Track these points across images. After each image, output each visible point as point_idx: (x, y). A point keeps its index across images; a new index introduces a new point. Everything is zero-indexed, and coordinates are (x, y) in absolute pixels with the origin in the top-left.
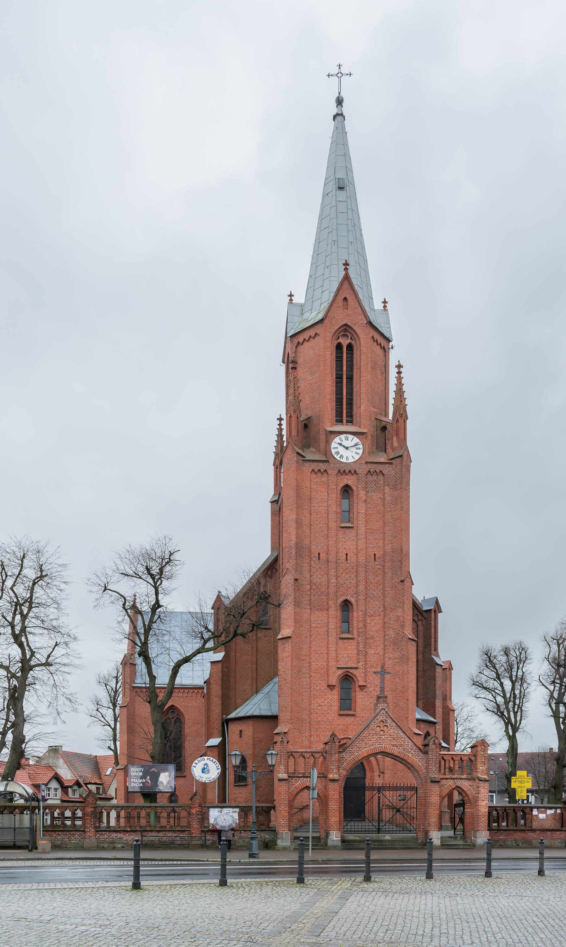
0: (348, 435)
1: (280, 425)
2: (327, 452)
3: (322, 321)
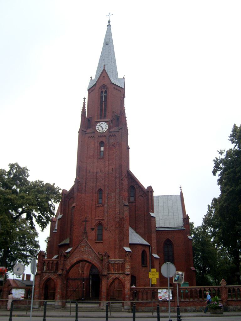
1: (84, 101)
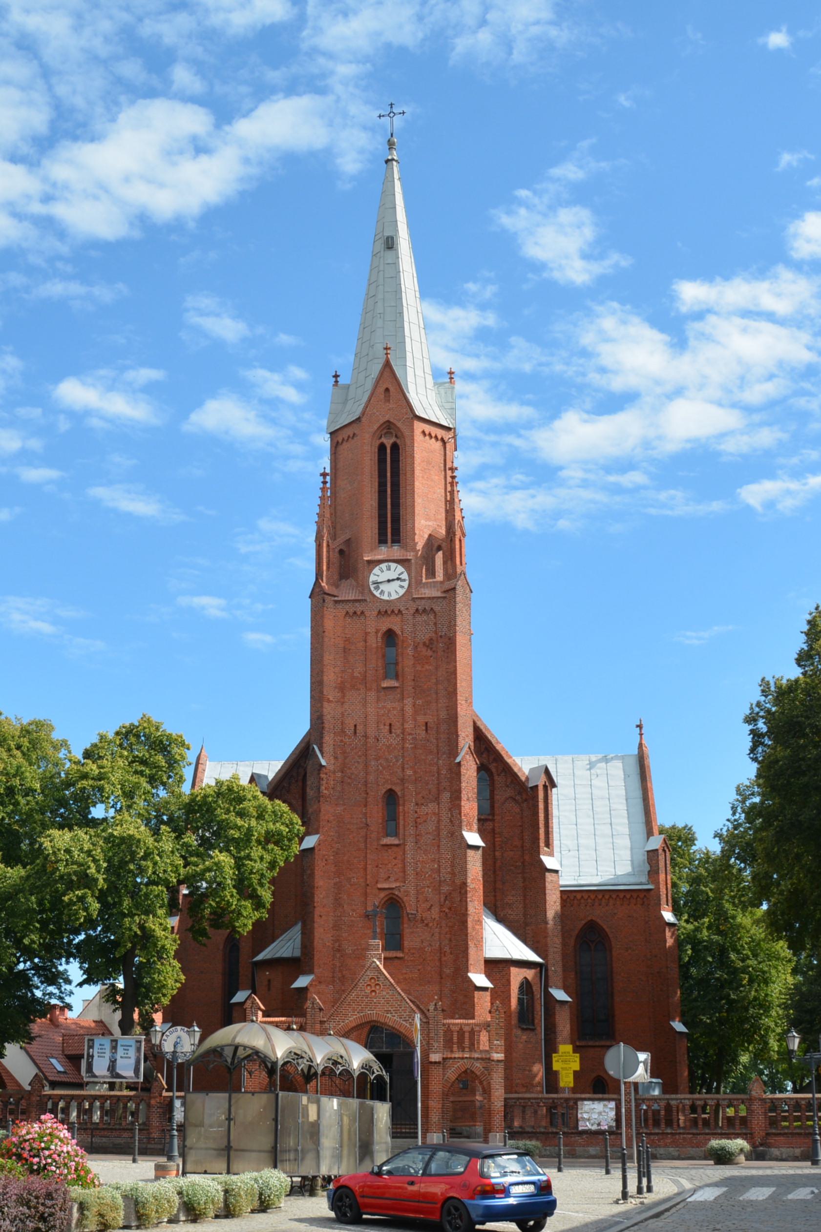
0: (390, 564)
2: (363, 587)
3: (358, 420)
